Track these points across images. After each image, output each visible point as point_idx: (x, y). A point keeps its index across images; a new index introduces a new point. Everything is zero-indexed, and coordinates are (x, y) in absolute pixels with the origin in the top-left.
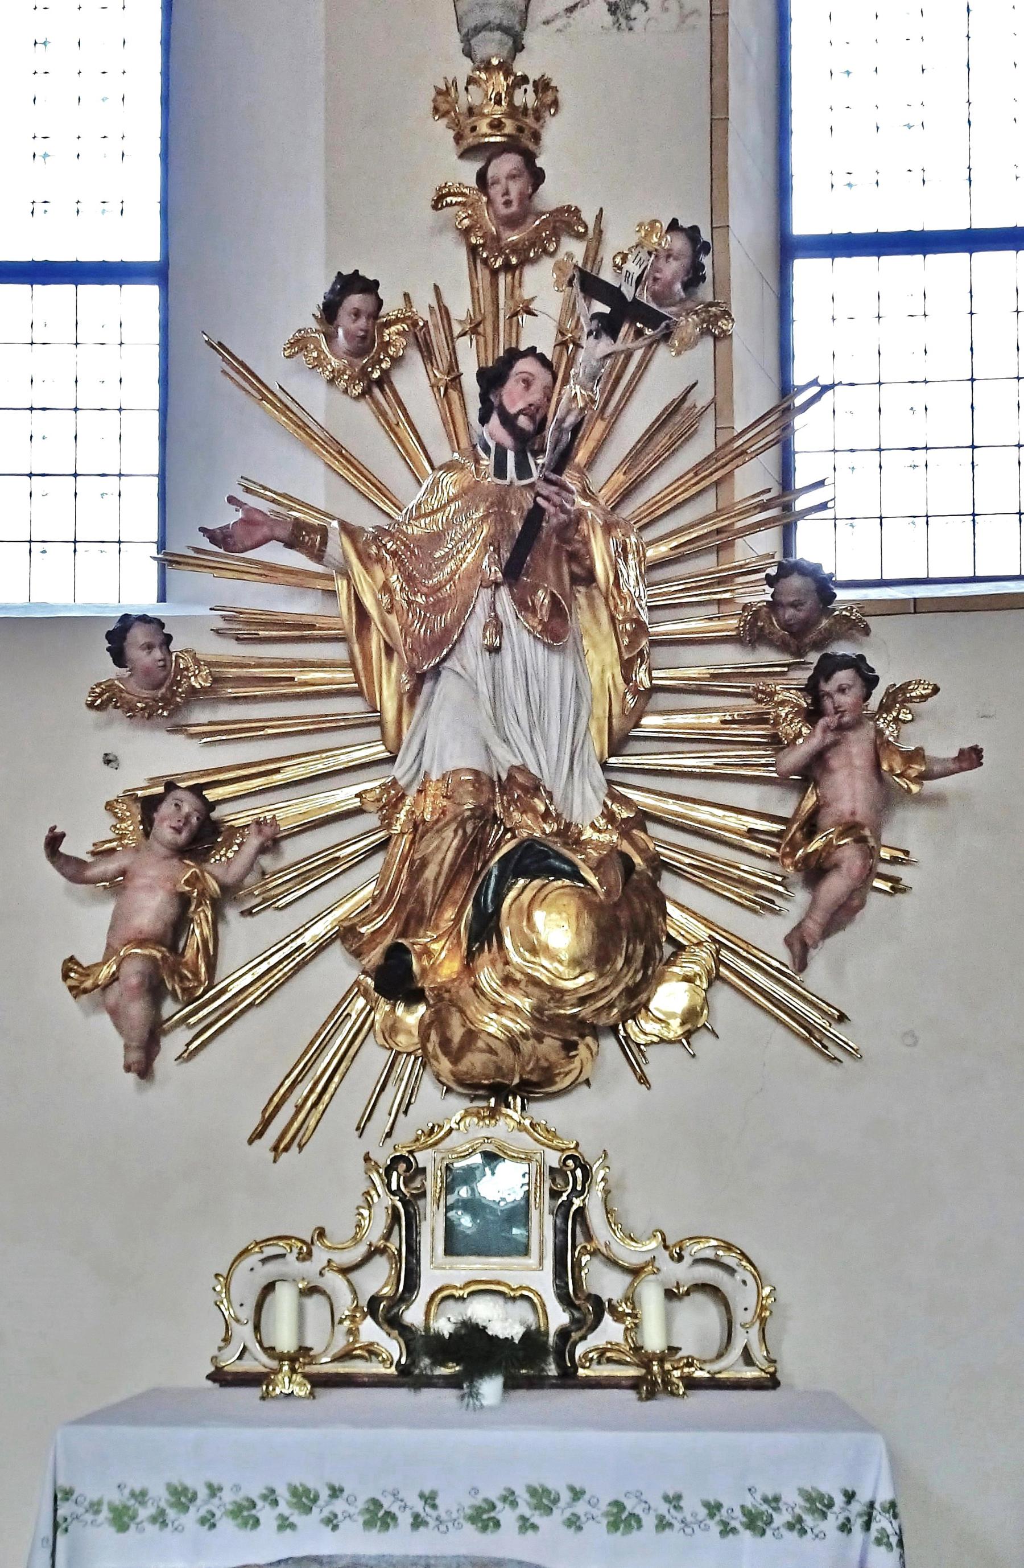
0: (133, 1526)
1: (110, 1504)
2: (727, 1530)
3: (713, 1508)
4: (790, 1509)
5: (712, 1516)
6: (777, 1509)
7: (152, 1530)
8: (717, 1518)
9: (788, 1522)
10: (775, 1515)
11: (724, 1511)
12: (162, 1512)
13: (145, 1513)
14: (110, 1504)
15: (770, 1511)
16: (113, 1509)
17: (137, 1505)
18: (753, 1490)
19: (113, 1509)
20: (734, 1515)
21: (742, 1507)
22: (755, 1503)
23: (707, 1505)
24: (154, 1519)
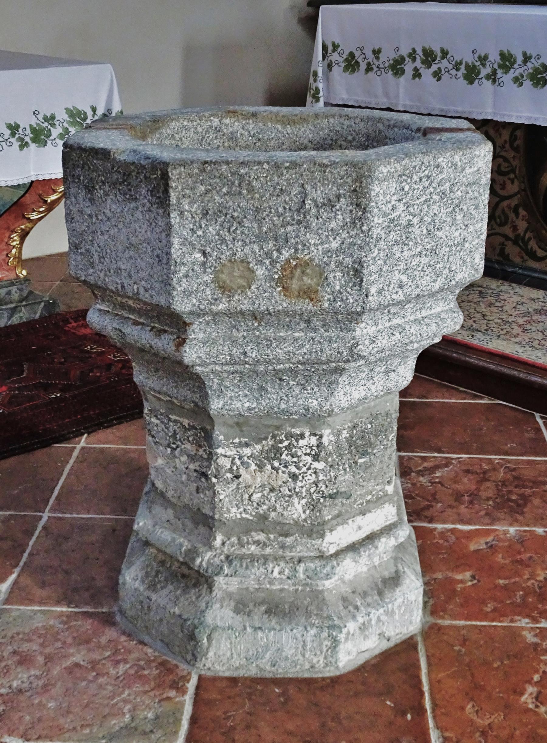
0: (49, 143)
1: (466, 63)
2: (23, 145)
3: (14, 129)
4: (61, 125)
5: (13, 135)
6: (53, 125)
7: (488, 84)
8: (17, 136)
9: (61, 134)
10: (52, 129)
11: (20, 130)
12: (494, 72)
13: (484, 72)
14: (466, 63)
15: (49, 127)
16: (467, 66)
17: (481, 66)
18: (37, 112)
19: (467, 66)
20: (27, 133)
21: (31, 125)
22: (38, 122)
23: (9, 126)
24: (488, 77)
